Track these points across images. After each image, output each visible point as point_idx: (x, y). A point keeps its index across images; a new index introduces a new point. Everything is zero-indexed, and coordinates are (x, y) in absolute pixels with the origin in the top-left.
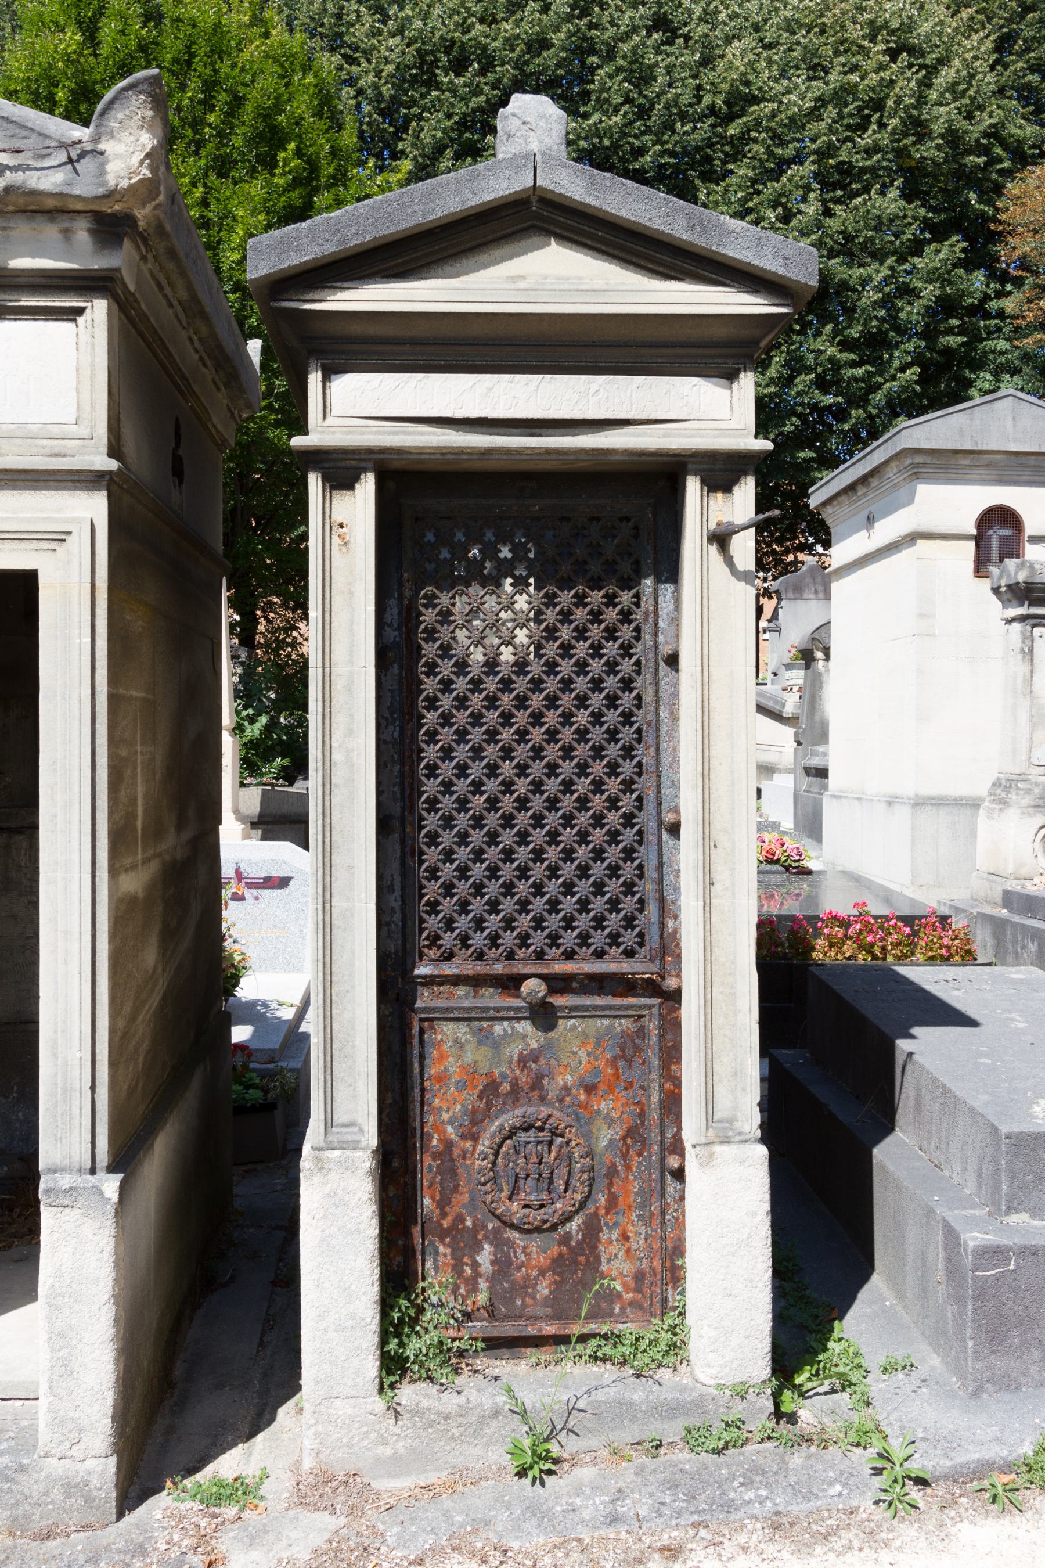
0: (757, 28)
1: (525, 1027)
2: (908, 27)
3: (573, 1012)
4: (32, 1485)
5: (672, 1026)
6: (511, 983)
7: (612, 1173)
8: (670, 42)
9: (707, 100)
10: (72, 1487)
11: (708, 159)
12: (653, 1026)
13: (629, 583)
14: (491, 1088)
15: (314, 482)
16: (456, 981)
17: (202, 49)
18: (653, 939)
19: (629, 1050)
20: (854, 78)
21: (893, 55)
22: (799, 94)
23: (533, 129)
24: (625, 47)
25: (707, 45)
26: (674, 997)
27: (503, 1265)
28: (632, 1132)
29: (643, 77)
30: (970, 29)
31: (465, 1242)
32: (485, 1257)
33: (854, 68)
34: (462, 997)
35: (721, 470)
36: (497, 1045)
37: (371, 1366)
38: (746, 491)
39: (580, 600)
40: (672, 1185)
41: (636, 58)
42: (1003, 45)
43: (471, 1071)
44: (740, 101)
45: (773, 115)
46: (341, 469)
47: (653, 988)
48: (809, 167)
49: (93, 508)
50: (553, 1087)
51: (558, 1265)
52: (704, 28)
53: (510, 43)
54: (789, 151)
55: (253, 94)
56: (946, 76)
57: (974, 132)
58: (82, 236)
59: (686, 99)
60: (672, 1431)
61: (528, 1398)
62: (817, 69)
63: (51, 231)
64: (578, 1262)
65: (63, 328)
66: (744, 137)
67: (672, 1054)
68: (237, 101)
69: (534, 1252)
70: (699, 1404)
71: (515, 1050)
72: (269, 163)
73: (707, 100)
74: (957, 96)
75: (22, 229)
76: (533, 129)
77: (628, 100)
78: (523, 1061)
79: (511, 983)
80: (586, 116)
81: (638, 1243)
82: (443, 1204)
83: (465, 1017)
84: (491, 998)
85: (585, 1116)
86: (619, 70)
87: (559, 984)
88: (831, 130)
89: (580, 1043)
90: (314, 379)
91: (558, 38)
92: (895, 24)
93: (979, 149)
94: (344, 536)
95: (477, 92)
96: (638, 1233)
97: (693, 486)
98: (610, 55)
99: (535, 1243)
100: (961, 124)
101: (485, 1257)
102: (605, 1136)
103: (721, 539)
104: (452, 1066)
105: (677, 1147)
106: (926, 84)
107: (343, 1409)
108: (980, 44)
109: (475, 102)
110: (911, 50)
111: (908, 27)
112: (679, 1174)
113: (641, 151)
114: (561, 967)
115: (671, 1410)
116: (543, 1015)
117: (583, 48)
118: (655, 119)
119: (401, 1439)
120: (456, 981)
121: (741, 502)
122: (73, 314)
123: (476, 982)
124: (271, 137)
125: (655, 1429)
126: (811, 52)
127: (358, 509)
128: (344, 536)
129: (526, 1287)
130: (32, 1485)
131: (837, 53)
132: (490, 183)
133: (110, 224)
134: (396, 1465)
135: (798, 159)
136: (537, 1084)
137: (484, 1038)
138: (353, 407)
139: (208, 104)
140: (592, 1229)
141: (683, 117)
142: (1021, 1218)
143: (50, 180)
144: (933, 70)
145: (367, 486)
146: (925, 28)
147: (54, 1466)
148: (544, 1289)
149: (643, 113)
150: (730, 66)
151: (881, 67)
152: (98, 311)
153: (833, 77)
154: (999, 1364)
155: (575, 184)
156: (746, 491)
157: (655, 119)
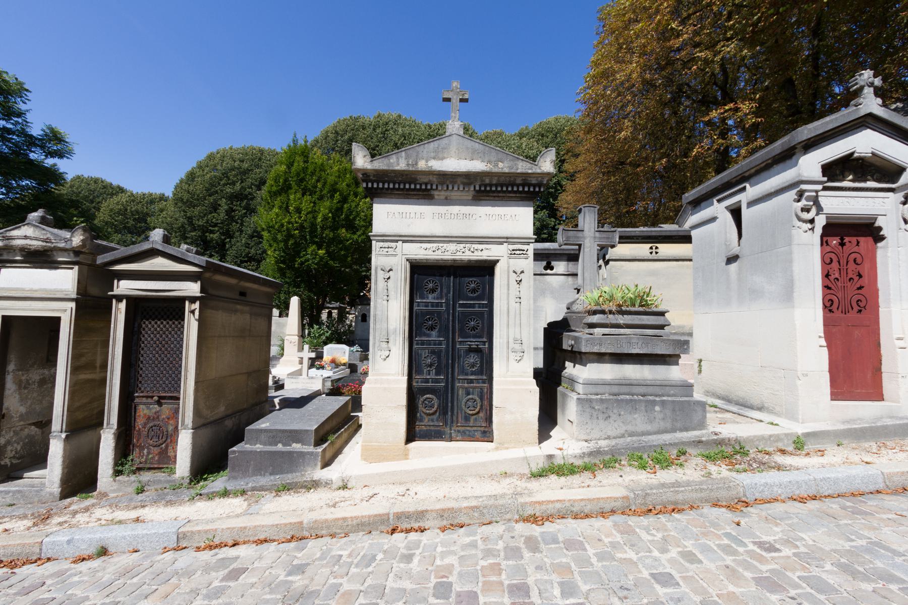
4: (43, 493)
6: (152, 397)
7: (171, 435)
10: (51, 494)
15: (114, 301)
27: (149, 453)
31: (142, 448)
32: (145, 451)
34: (144, 400)
35: (193, 300)
36: (150, 409)
37: (111, 472)
38: (198, 303)
43: (145, 415)
46: (119, 298)
49: (73, 305)
50: (161, 418)
51: (160, 454)
55: (329, 181)
57: (551, 183)
58: (72, 255)
63: (66, 254)
68: (325, 183)
71: (154, 411)
72: (332, 197)
75: (60, 253)
76: (157, 235)
78: (155, 413)
79: (152, 397)
82: (138, 441)
84: (149, 400)
87: (160, 398)
90: (116, 281)
94: (120, 312)
97: (187, 303)
99: (156, 449)
101: (145, 451)
103: (193, 312)
104: (142, 414)
116: (159, 403)
119: (115, 486)
121: (197, 306)
122: (72, 268)
123: (147, 397)
124: (333, 190)
127: (123, 306)
128: (120, 312)
130: (43, 493)
132: (146, 246)
133: (77, 252)
134: (114, 491)
136: (158, 417)
137: (148, 408)
138: (124, 287)
140: (167, 447)
145: (124, 301)
147: (48, 490)
148: (156, 458)
152: (76, 268)
154: (233, 474)
156: (198, 303)
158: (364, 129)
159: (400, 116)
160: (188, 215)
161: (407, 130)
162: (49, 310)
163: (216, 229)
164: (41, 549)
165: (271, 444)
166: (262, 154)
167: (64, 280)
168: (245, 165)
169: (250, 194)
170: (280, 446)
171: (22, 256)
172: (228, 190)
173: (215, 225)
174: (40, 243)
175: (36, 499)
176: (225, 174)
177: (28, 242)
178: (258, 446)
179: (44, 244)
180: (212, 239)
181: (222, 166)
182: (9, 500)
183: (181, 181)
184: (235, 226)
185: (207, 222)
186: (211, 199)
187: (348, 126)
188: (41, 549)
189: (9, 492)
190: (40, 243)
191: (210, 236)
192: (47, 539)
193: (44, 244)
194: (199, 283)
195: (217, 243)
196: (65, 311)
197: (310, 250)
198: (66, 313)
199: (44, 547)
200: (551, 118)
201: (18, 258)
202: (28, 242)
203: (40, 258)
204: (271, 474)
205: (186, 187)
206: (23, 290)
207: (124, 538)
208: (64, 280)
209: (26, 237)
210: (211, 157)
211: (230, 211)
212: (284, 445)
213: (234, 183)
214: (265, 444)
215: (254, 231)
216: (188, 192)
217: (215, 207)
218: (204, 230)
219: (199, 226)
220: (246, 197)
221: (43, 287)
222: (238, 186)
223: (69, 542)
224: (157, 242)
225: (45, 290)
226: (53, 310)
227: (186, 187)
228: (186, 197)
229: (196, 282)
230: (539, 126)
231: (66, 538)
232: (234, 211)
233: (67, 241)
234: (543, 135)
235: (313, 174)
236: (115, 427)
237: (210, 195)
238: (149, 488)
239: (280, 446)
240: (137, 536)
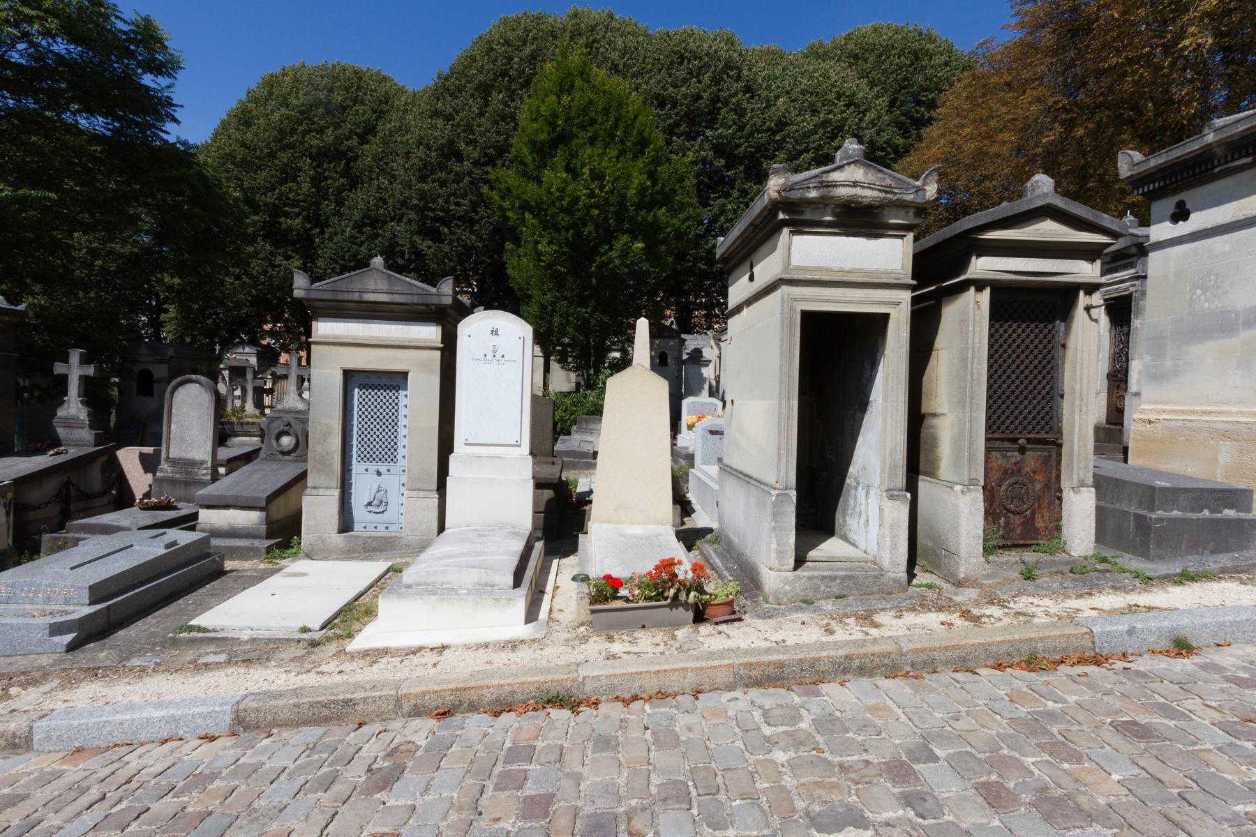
0: (788, 93)
1: (1016, 454)
2: (854, 94)
3: (1031, 450)
5: (1059, 455)
6: (1015, 441)
8: (752, 97)
9: (768, 124)
10: (896, 581)
11: (767, 150)
12: (1054, 455)
13: (1052, 321)
14: (1006, 471)
16: (997, 439)
17: (615, 104)
18: (1056, 429)
19: (1046, 461)
20: (831, 116)
21: (848, 106)
22: (807, 122)
23: (1042, 186)
24: (734, 100)
25: (768, 101)
26: (1060, 446)
27: (1007, 524)
28: (1046, 485)
29: (741, 113)
30: (877, 97)
32: (1002, 521)
33: (830, 112)
39: (1045, 327)
40: (1057, 502)
41: (738, 104)
42: (892, 104)
43: (1000, 466)
44: (782, 124)
45: (797, 131)
47: (1054, 443)
48: (811, 155)
51: (1023, 524)
52: (766, 93)
53: (685, 96)
54: (803, 147)
56: (870, 116)
58: (911, 213)
59: (759, 123)
60: (1066, 569)
61: (1026, 559)
62: (815, 112)
63: (902, 212)
64: (1029, 524)
65: (899, 241)
66: (784, 140)
67: (1059, 462)
69: (1016, 520)
70: (1074, 561)
71: (1013, 460)
73: (768, 124)
74: (874, 125)
77: (735, 123)
80: (716, 129)
81: (1046, 518)
83: (1000, 450)
84: (1007, 445)
85: (1032, 481)
86: (731, 110)
87: (1029, 441)
88: (821, 139)
89: (1032, 459)
91: (705, 95)
92: (848, 93)
93: (883, 149)
95: (670, 118)
96: (1047, 515)
97: (1082, 293)
98: (726, 103)
99: (1016, 518)
100: (875, 138)
101: (1002, 521)
102: (1038, 486)
105: (1060, 490)
106: (861, 120)
107: (973, 560)
108: (883, 102)
109: (669, 122)
110: (854, 104)
111: (854, 94)
112: (1060, 499)
113: (738, 146)
114: (1031, 436)
115: (1066, 563)
116: (1022, 450)
117: (715, 99)
118: (746, 131)
119: (989, 569)
120: (997, 439)
122: (902, 237)
123: (1003, 440)
125: (1061, 568)
126: (812, 104)
129: (1014, 529)
131: (824, 105)
133: (921, 210)
134: (987, 577)
135: (807, 151)
136: (1019, 471)
137: (1005, 457)
138: (981, 266)
139: (616, 127)
140: (1033, 514)
141: (759, 132)
142: (1160, 512)
143: (909, 197)
144: (864, 113)
146: (861, 95)
148: (1019, 531)
149: (742, 129)
150: (778, 110)
151: (844, 112)
153: (822, 115)
155: (1060, 202)
157: (746, 131)
158: (555, 37)
159: (611, 16)
160: (246, 184)
161: (632, 41)
162: (873, 303)
163: (297, 210)
164: (1093, 643)
165: (1193, 510)
166: (360, 78)
167: (891, 255)
168: (338, 98)
169: (350, 149)
170: (1206, 513)
171: (834, 214)
172: (315, 142)
173: (295, 203)
174: (876, 194)
175: (875, 589)
176: (306, 112)
177: (858, 191)
178: (1175, 512)
179: (882, 195)
180: (290, 229)
181: (297, 97)
182: (836, 590)
183: (224, 125)
184: (328, 207)
185: (279, 198)
186: (284, 157)
187: (527, 31)
188: (1093, 643)
189: (836, 578)
190: (876, 194)
191: (285, 223)
192: (43, 723)
193: (882, 195)
194: (1098, 263)
195: (298, 234)
196: (898, 304)
197: (618, 245)
198: (898, 309)
199: (1097, 639)
200: (866, 27)
201: (828, 218)
202: (858, 191)
203: (859, 219)
204: (1212, 552)
205: (236, 135)
206: (830, 270)
207: (1205, 626)
208: (891, 255)
209: (855, 184)
210: (271, 83)
211: (316, 181)
212: (1212, 511)
213: (321, 131)
214: (1185, 510)
215: (365, 216)
216: (244, 145)
217: (289, 174)
218: (276, 212)
219: (266, 204)
220: (344, 154)
221: (857, 266)
222: (330, 136)
223: (1131, 632)
224: (1045, 195)
225: (867, 273)
226: (873, 303)
227: (236, 135)
228: (240, 153)
229: (1092, 260)
230: (848, 38)
231: (1126, 627)
232: (326, 179)
233: (919, 190)
234: (856, 57)
235: (606, 111)
236: (795, 499)
237: (283, 149)
238: (1038, 572)
239: (1206, 513)
240: (1223, 624)
